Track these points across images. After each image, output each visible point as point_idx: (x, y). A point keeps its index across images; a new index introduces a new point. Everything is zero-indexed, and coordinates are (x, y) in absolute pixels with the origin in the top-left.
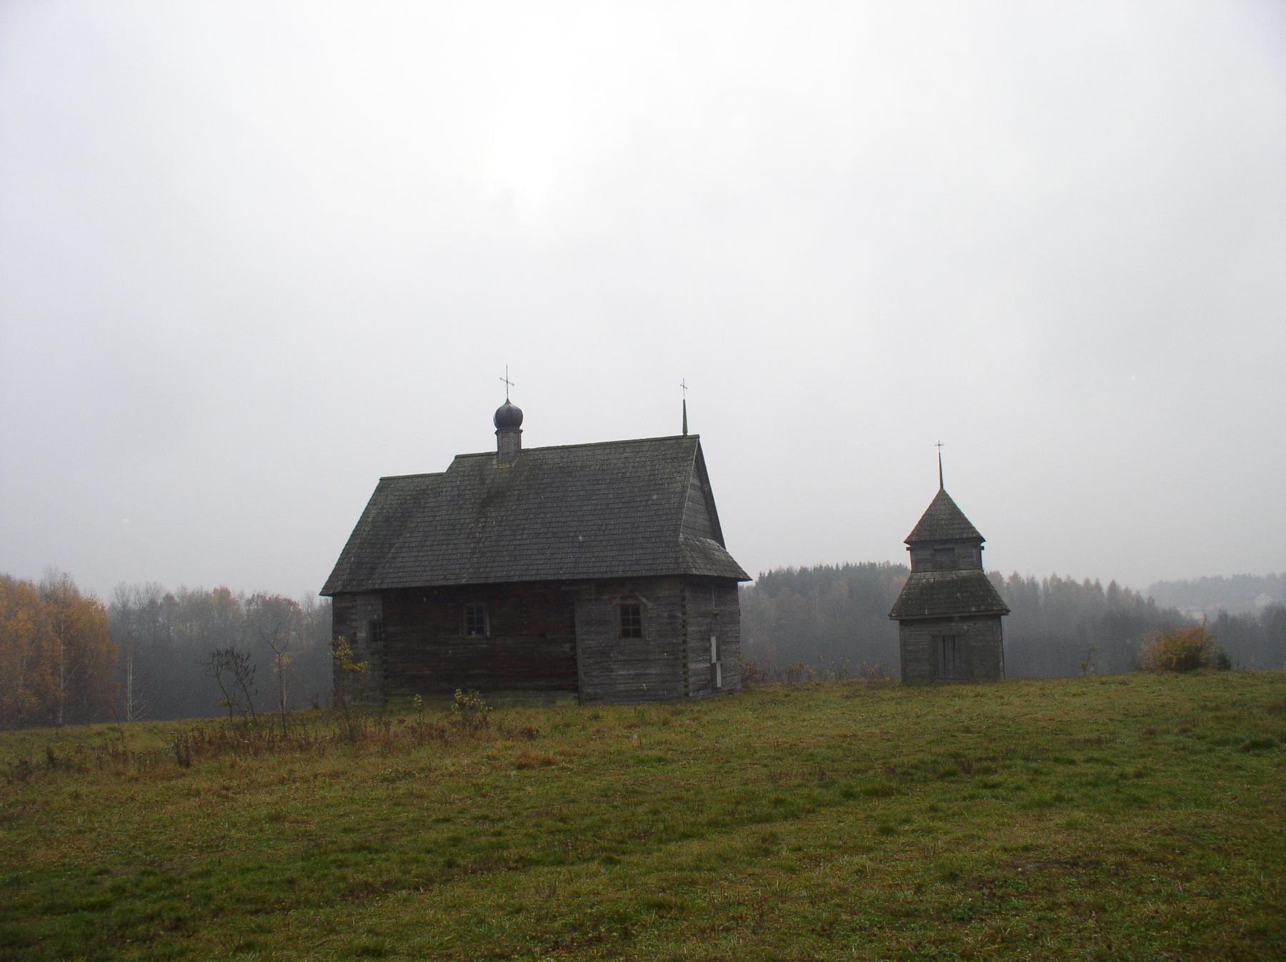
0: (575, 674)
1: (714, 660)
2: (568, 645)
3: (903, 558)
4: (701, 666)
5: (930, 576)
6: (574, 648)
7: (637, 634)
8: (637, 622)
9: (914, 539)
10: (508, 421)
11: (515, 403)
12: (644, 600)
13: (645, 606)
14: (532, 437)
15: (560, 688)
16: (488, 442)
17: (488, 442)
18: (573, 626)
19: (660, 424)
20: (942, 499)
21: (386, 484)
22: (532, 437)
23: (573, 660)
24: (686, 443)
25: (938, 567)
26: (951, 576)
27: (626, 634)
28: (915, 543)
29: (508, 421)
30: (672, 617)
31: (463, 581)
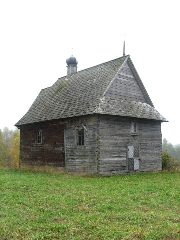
0: (64, 160)
1: (131, 154)
2: (62, 148)
6: (63, 149)
8: (83, 138)
10: (72, 63)
12: (84, 127)
13: (85, 130)
14: (80, 67)
29: (72, 63)
30: (94, 135)
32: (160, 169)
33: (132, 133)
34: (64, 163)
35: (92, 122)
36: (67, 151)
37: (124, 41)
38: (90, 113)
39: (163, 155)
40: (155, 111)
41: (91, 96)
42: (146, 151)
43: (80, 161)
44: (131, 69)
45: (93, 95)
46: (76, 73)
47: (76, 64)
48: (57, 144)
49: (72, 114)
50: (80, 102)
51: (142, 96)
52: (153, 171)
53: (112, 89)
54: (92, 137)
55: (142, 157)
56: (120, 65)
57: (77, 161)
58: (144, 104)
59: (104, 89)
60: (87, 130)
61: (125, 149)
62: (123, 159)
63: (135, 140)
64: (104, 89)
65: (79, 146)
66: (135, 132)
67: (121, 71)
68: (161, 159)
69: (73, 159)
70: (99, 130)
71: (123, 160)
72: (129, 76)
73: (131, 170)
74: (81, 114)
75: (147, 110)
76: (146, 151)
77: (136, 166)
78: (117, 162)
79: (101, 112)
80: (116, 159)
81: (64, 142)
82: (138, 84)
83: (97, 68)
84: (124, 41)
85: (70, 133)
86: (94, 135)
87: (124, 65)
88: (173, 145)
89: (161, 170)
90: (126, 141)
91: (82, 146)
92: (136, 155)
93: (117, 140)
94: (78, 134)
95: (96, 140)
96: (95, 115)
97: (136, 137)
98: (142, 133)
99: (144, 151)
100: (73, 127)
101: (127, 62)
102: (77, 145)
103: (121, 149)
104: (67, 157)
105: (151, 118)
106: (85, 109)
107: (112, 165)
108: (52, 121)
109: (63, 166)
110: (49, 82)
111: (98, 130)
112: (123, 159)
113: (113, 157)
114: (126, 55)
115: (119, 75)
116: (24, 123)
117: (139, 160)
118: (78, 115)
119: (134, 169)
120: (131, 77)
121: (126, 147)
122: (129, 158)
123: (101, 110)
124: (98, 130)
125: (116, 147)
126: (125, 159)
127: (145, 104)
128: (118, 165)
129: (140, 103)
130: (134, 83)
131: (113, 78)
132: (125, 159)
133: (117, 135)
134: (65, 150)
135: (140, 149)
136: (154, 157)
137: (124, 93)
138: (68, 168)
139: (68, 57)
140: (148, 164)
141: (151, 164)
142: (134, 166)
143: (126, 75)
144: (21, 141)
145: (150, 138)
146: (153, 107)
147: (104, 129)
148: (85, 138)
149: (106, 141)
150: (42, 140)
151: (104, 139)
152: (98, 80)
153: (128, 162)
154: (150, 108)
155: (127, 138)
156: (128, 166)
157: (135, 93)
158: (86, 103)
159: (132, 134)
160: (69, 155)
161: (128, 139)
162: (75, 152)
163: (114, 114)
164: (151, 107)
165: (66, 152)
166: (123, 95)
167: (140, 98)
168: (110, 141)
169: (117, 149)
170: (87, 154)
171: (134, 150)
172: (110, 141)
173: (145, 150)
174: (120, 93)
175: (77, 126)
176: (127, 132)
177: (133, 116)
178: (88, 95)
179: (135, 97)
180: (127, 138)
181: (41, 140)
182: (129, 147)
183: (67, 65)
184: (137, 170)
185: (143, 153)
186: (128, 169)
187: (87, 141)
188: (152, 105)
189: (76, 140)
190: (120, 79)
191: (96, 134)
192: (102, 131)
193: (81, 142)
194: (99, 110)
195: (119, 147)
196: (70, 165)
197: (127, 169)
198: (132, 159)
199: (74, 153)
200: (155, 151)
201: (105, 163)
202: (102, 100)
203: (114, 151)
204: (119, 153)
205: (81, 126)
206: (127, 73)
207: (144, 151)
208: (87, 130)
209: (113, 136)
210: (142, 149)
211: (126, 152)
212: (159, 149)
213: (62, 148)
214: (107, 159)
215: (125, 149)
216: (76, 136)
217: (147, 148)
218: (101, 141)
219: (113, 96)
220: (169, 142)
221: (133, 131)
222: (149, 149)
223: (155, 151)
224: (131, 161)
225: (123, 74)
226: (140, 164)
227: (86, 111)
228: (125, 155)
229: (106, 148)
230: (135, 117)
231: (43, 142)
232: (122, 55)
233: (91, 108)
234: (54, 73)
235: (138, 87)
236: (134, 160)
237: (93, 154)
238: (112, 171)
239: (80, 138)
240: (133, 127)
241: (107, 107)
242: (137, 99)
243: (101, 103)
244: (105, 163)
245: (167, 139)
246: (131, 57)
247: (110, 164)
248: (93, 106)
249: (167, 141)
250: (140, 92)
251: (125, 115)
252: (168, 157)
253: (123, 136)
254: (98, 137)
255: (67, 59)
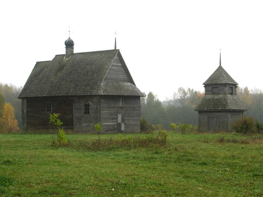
0: (73, 124)
1: (120, 120)
2: (71, 116)
3: (202, 90)
4: (105, 124)
5: (209, 97)
6: (72, 117)
7: (88, 113)
8: (88, 109)
9: (206, 83)
10: (69, 44)
11: (72, 38)
12: (90, 102)
13: (90, 104)
14: (77, 49)
15: (69, 129)
16: (63, 51)
17: (63, 51)
18: (72, 110)
19: (104, 45)
20: (220, 71)
21: (38, 64)
22: (77, 49)
23: (72, 120)
24: (115, 52)
25: (213, 93)
26: (216, 97)
27: (86, 113)
28: (207, 85)
29: (69, 44)
30: (97, 108)
31: (44, 95)
32: (139, 130)
33: (120, 106)
34: (73, 127)
35: (95, 100)
36: (75, 118)
37: (116, 38)
38: (95, 94)
39: (142, 120)
40: (136, 89)
41: (93, 80)
42: (129, 118)
43: (87, 125)
44: (120, 59)
45: (95, 80)
46: (73, 54)
47: (73, 45)
48: (66, 113)
49: (80, 93)
50: (85, 84)
51: (127, 78)
52: (134, 132)
53: (108, 76)
54: (95, 109)
55: (126, 122)
56: (113, 58)
57: (84, 125)
58: (129, 84)
59: (103, 76)
60: (91, 104)
61: (116, 117)
62: (114, 123)
63: (122, 110)
64: (103, 76)
65: (85, 115)
66: (122, 105)
67: (114, 62)
68: (140, 123)
69: (81, 124)
70: (101, 105)
71: (115, 124)
72: (118, 64)
73: (120, 131)
74: (88, 94)
75: (131, 88)
76: (129, 118)
77: (123, 128)
78: (111, 125)
79: (102, 94)
80: (110, 123)
81: (73, 112)
82: (124, 69)
83: (94, 54)
84: (116, 38)
85: (79, 106)
86: (97, 108)
87: (116, 57)
88: (161, 101)
89: (139, 131)
90: (117, 111)
91: (88, 115)
92: (123, 120)
93: (111, 111)
94: (84, 106)
95: (99, 111)
96: (99, 95)
97: (123, 108)
98: (127, 105)
99: (128, 118)
100: (80, 101)
101: (118, 54)
102: (84, 114)
103: (113, 117)
104: (75, 122)
105: (134, 95)
106: (91, 91)
107: (108, 127)
108: (62, 97)
109: (72, 129)
110: (49, 57)
111: (100, 105)
112: (114, 123)
113: (108, 122)
114: (117, 49)
115: (112, 65)
116: (34, 96)
117: (125, 124)
118: (86, 94)
119: (122, 130)
120: (120, 65)
121: (117, 115)
122: (119, 122)
123: (102, 92)
124: (100, 105)
125: (110, 115)
126: (116, 123)
127: (129, 84)
128: (112, 127)
129: (126, 83)
130: (122, 69)
131: (108, 68)
132: (116, 123)
133: (111, 108)
134: (74, 117)
135: (125, 116)
136: (135, 122)
137: (115, 78)
138: (76, 130)
139: (66, 39)
140: (131, 127)
141: (133, 127)
142: (122, 128)
143: (117, 64)
144: (29, 109)
145: (132, 109)
146: (135, 85)
147: (104, 104)
148: (90, 110)
149: (105, 112)
150: (52, 110)
151: (103, 110)
152: (97, 67)
153: (118, 126)
154: (133, 87)
155: (117, 109)
156: (118, 128)
157: (123, 76)
158: (90, 86)
159: (120, 107)
160: (77, 121)
161: (117, 110)
162: (82, 119)
163: (110, 94)
164: (133, 86)
165: (74, 119)
166: (114, 79)
167: (126, 79)
168: (107, 112)
169: (111, 117)
170: (92, 120)
171: (122, 117)
172: (107, 112)
173: (129, 117)
174: (113, 78)
175: (84, 101)
176: (117, 105)
177: (121, 94)
178: (90, 79)
179: (122, 79)
180: (117, 109)
181: (51, 110)
182: (118, 115)
183: (65, 47)
184: (124, 131)
185: (128, 119)
186: (118, 130)
187: (91, 111)
188: (134, 84)
189: (83, 111)
190: (113, 68)
191: (99, 107)
192: (102, 105)
193: (87, 111)
194: (101, 93)
195: (112, 115)
196: (78, 128)
197: (117, 130)
198: (120, 124)
199: (81, 120)
200: (135, 118)
201: (104, 126)
202: (102, 85)
203: (109, 118)
204: (112, 119)
205: (88, 102)
206: (117, 63)
207: (128, 118)
208: (91, 104)
209: (109, 108)
210: (127, 116)
211: (117, 119)
212: (139, 117)
213: (71, 116)
214: (105, 124)
215: (116, 117)
216: (83, 108)
217: (130, 116)
218: (102, 112)
219: (108, 80)
220: (156, 99)
221: (121, 104)
222: (131, 117)
223: (135, 118)
224: (119, 125)
225: (115, 64)
226: (125, 127)
227: (92, 92)
228: (116, 121)
229: (104, 117)
230: (122, 95)
231: (53, 111)
232: (114, 49)
233: (95, 90)
234: (51, 50)
235: (125, 72)
236: (122, 124)
237: (96, 120)
238: (108, 131)
239: (86, 109)
240: (121, 102)
241: (106, 90)
242: (124, 81)
243: (102, 87)
244: (104, 126)
245: (154, 94)
246: (120, 51)
247: (107, 126)
248: (97, 89)
249: (154, 96)
250: (126, 75)
251: (116, 94)
252: (145, 122)
253: (115, 108)
254: (100, 109)
255: (65, 40)
